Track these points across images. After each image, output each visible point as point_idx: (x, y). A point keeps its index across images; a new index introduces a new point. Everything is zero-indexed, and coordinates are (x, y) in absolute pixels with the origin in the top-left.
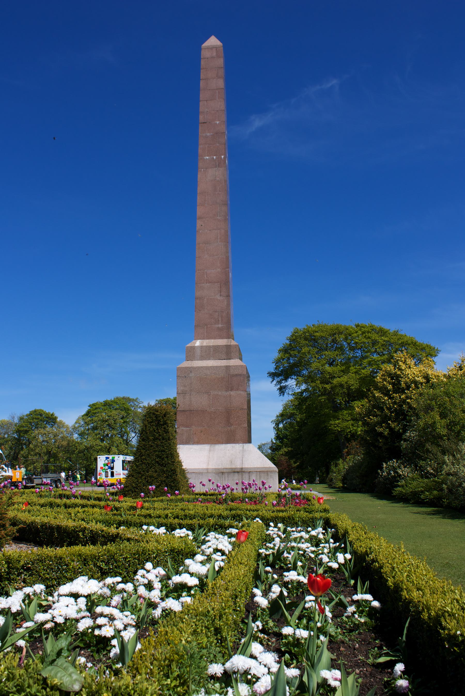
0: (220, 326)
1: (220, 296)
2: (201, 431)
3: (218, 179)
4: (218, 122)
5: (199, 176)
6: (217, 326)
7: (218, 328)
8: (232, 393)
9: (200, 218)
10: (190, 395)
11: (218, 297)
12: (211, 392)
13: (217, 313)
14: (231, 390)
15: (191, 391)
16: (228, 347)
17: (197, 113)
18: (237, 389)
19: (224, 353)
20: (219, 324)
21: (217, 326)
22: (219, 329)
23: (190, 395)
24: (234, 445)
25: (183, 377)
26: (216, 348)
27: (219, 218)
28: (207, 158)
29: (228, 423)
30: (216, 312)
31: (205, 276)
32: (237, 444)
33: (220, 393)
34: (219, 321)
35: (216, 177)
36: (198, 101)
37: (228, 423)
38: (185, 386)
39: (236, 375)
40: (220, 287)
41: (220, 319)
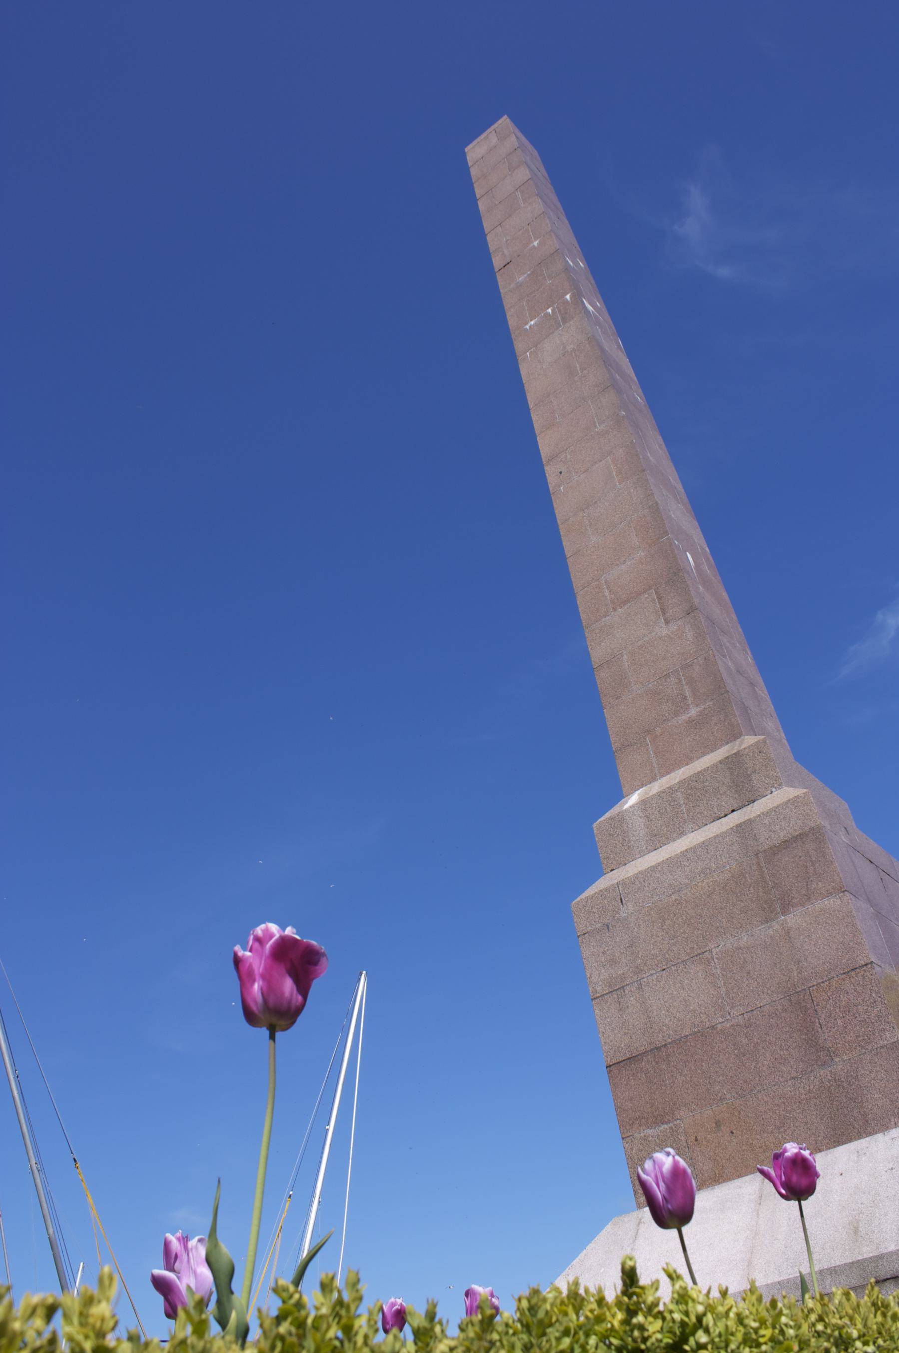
0: (693, 712)
1: (667, 622)
2: (718, 1124)
3: (570, 348)
4: (536, 244)
5: (524, 372)
6: (684, 718)
7: (690, 721)
8: (792, 919)
9: (552, 458)
10: (640, 988)
11: (663, 630)
12: (711, 945)
13: (673, 680)
14: (785, 911)
15: (638, 970)
16: (733, 763)
17: (485, 255)
18: (808, 898)
19: (724, 789)
20: (687, 708)
21: (684, 718)
22: (695, 724)
23: (640, 988)
24: (863, 1143)
25: (598, 931)
26: (694, 788)
27: (600, 428)
28: (532, 323)
29: (817, 1051)
30: (668, 676)
31: (607, 593)
32: (879, 1136)
33: (745, 940)
34: (685, 698)
35: (565, 348)
36: (483, 236)
37: (817, 1051)
38: (613, 962)
39: (786, 844)
40: (659, 598)
41: (688, 693)
